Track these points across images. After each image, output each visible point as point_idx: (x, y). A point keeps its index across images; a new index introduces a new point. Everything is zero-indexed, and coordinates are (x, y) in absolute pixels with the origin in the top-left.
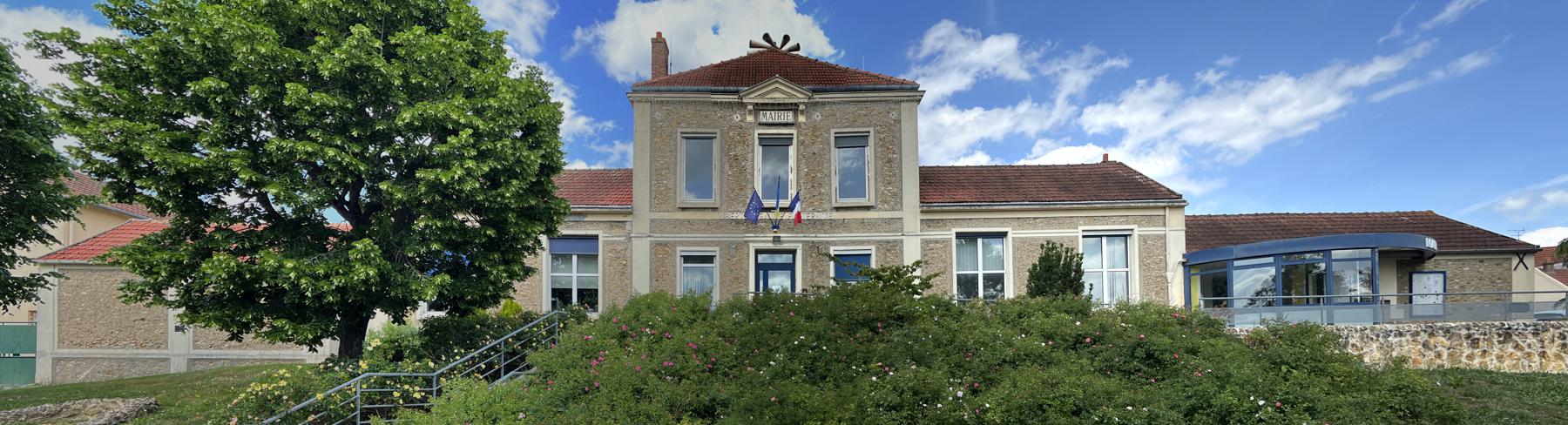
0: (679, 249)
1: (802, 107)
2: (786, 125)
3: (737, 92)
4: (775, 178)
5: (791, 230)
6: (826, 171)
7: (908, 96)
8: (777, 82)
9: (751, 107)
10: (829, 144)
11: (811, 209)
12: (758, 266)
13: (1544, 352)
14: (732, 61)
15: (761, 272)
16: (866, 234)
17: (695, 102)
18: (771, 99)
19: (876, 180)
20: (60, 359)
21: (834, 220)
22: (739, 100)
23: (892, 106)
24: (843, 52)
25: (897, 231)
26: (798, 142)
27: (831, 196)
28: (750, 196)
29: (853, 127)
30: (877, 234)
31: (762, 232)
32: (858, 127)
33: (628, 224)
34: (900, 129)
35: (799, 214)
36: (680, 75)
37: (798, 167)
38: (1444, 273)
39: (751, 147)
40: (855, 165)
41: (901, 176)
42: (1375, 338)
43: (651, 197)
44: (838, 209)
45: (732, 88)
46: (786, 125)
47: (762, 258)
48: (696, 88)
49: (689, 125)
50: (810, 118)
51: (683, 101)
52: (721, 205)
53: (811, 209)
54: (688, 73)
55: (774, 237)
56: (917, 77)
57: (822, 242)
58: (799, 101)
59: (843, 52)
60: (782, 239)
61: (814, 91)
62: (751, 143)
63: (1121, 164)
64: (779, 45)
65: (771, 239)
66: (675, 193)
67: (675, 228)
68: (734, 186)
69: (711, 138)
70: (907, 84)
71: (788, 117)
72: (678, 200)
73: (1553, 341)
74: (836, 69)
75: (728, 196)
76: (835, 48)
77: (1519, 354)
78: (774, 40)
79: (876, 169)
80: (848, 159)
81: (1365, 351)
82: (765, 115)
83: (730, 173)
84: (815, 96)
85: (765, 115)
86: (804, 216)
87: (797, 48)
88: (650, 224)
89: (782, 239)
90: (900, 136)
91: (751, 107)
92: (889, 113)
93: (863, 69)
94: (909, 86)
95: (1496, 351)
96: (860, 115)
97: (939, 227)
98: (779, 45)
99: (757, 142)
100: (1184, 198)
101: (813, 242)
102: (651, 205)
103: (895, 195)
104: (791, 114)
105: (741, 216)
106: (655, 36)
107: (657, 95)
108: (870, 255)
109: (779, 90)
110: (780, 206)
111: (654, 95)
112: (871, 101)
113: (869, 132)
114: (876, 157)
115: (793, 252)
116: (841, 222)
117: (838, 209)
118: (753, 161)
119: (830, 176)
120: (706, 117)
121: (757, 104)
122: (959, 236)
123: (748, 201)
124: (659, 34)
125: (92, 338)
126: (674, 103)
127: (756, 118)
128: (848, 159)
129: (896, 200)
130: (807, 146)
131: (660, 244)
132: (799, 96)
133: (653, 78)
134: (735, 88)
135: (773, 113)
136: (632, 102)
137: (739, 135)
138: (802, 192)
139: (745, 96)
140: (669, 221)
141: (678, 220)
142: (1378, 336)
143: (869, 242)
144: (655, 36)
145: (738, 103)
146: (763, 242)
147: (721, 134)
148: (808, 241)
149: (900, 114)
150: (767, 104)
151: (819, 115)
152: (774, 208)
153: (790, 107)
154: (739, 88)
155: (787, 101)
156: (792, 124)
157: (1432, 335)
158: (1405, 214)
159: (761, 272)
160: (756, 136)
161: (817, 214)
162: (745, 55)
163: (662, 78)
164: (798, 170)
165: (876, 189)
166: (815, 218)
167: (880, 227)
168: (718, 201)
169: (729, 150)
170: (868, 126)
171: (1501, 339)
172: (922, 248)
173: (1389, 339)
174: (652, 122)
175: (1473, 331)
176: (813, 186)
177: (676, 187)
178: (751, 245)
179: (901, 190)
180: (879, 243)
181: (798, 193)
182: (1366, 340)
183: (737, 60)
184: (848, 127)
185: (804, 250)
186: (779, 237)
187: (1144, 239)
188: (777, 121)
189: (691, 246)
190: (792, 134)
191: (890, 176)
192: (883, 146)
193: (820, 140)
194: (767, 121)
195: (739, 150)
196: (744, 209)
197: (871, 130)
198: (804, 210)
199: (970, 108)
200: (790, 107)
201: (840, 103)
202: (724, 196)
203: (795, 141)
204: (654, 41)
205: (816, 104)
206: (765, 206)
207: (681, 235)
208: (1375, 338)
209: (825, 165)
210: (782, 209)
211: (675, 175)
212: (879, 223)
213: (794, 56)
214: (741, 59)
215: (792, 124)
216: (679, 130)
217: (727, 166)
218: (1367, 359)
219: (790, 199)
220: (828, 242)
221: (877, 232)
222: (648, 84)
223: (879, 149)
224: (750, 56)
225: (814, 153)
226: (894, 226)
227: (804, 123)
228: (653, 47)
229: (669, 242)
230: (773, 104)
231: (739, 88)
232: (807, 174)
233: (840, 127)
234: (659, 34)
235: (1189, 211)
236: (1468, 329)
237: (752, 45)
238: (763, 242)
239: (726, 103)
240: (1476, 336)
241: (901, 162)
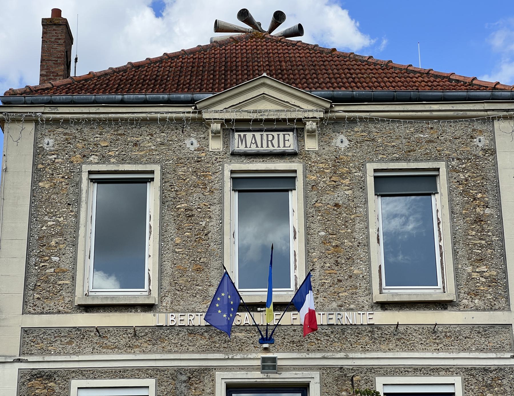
1: (310, 125)
2: (282, 155)
3: (192, 102)
4: (264, 248)
5: (297, 345)
6: (360, 237)
7: (507, 110)
8: (264, 85)
9: (216, 127)
10: (364, 189)
11: (334, 305)
14: (184, 53)
16: (441, 355)
17: (116, 120)
18: (255, 112)
19: (455, 253)
21: (379, 327)
22: (196, 115)
23: (478, 126)
24: (385, 42)
26: (306, 184)
27: (370, 282)
28: (216, 283)
30: (462, 355)
31: (241, 350)
32: (416, 160)
34: (495, 164)
35: (311, 315)
36: (91, 77)
37: (307, 228)
39: (217, 194)
40: (410, 227)
41: (503, 247)
43: (26, 286)
44: (384, 306)
45: (182, 96)
46: (282, 155)
48: (119, 97)
49: (104, 159)
50: (329, 144)
51: (94, 120)
52: (161, 299)
53: (334, 305)
54: (105, 74)
55: (264, 360)
57: (358, 369)
58: (306, 115)
59: (385, 42)
60: (279, 363)
61: (336, 100)
62: (217, 186)
64: (266, 27)
65: (259, 363)
66: (73, 278)
67: (70, 343)
68: (186, 264)
69: (145, 181)
70: (501, 90)
72: (79, 292)
74: (369, 64)
75: (174, 283)
76: (372, 38)
78: (256, 19)
79: (454, 234)
80: (395, 216)
82: (243, 140)
83: (178, 240)
84: (337, 108)
85: (243, 140)
86: (321, 319)
87: (299, 31)
88: (22, 337)
89: (279, 363)
90: (497, 177)
91: (216, 127)
92: (472, 137)
93: (420, 65)
96: (418, 141)
98: (266, 27)
99: (228, 184)
101: (341, 368)
102: (25, 303)
103: (492, 281)
104: (291, 137)
105: (199, 320)
106: (49, 16)
107: (47, 110)
110: (274, 300)
111: (42, 110)
112: (439, 118)
113: (438, 170)
114: (452, 212)
116: (392, 329)
117: (384, 306)
118: (222, 219)
119: (368, 245)
120: (136, 145)
121: (228, 121)
123: (212, 291)
124: (57, 12)
126: (78, 122)
127: (226, 144)
128: (395, 216)
130: (324, 191)
133: (42, 82)
134: (189, 96)
135: (258, 135)
138: (315, 275)
139: (207, 107)
140: (58, 331)
141: (78, 329)
143: (447, 370)
144: (49, 16)
145: (193, 119)
146: (242, 368)
147: (163, 174)
148: (330, 367)
149: (493, 140)
150: (247, 121)
151: (345, 139)
152: (262, 305)
153: (288, 125)
154: (197, 96)
155: (283, 116)
156: (293, 155)
160: (227, 174)
161: (346, 314)
162: (206, 42)
163: (58, 82)
164: (307, 234)
165: (456, 269)
166: (344, 322)
167: (470, 342)
168: (155, 294)
169: (177, 199)
170: (436, 159)
176: (337, 263)
177: (74, 269)
178: (219, 375)
179: (505, 272)
180: (320, 368)
181: (308, 276)
183: (192, 52)
184: (398, 160)
185: (323, 384)
186: (274, 359)
188: (264, 149)
189: (100, 377)
190: (295, 171)
191: (482, 247)
193: (347, 181)
194: (248, 150)
196: (205, 307)
197: (442, 166)
198: (322, 307)
200: (288, 125)
201: (382, 120)
202: (166, 283)
203: (299, 183)
204: (46, 23)
205: (338, 121)
206: (246, 300)
207: (81, 358)
209: (357, 226)
210: (280, 307)
211: (75, 245)
212: (467, 333)
213: (294, 44)
214: (200, 50)
215: (293, 155)
216: (86, 168)
217: (172, 228)
219: (293, 287)
220: (372, 369)
221: (464, 350)
222: (30, 91)
223: (458, 199)
224: (215, 45)
225: (337, 205)
226: (494, 340)
227: (316, 153)
228: (44, 33)
229: (56, 372)
230: (256, 121)
231: (197, 96)
232: (325, 241)
233: (382, 160)
234: (57, 12)
237: (218, 28)
238: (242, 368)
239: (171, 119)
241: (501, 222)
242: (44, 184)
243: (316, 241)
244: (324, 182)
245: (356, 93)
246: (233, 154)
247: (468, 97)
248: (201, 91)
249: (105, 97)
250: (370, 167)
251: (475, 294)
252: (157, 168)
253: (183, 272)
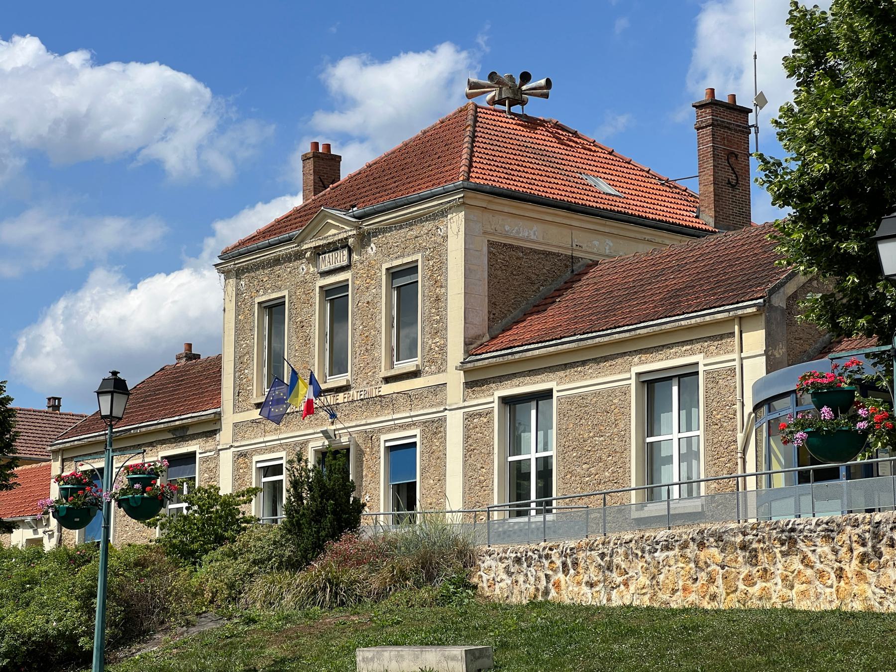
0: (383, 437)
13: (841, 569)
42: (640, 554)
56: (292, 204)
73: (851, 550)
77: (809, 572)
81: (630, 574)
88: (234, 430)
95: (779, 569)
97: (483, 391)
108: (415, 443)
117: (388, 380)
122: (506, 401)
142: (643, 551)
157: (702, 545)
171: (784, 548)
173: (656, 555)
174: (237, 295)
175: (750, 537)
182: (631, 557)
199: (58, 300)
208: (640, 554)
225: (368, 303)
235: (312, 397)
236: (745, 534)
240: (755, 545)
250: (418, 257)
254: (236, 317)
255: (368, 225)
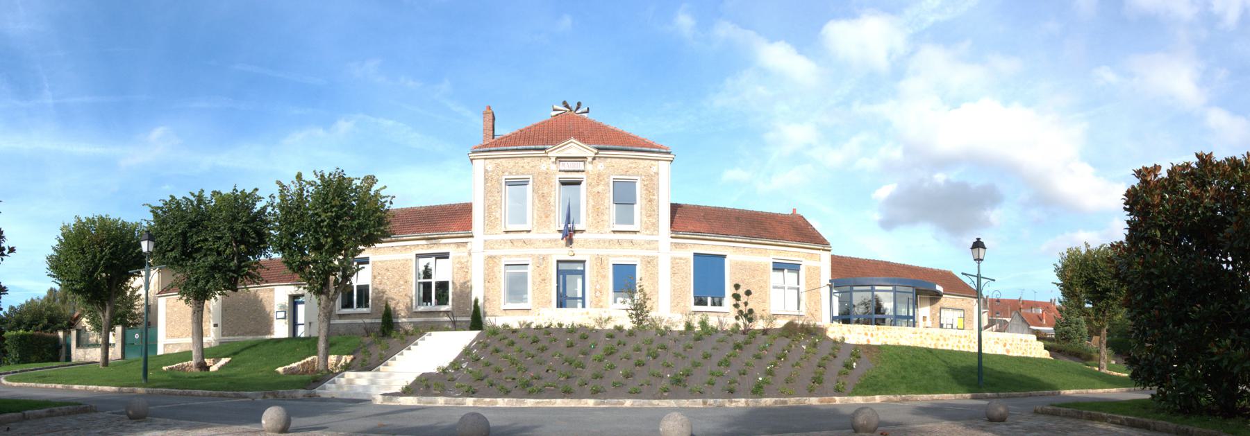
3: (544, 149)
12: (559, 272)
15: (561, 276)
20: (167, 344)
25: (654, 249)
29: (626, 175)
32: (629, 175)
33: (469, 244)
38: (940, 308)
39: (553, 187)
41: (658, 212)
43: (484, 224)
47: (563, 267)
48: (515, 147)
61: (599, 149)
63: (802, 217)
64: (574, 109)
69: (579, 183)
71: (580, 166)
94: (665, 151)
100: (831, 245)
102: (484, 231)
103: (653, 224)
109: (573, 148)
115: (583, 262)
125: (179, 334)
129: (655, 226)
130: (594, 187)
131: (490, 257)
132: (589, 152)
136: (472, 160)
137: (545, 178)
147: (533, 179)
154: (546, 146)
158: (940, 271)
159: (561, 276)
170: (528, 174)
172: (672, 262)
187: (808, 269)
192: (646, 190)
195: (545, 190)
197: (531, 177)
203: (531, 182)
217: (537, 201)
218: (458, 429)
225: (598, 192)
226: (652, 246)
231: (546, 146)
233: (616, 175)
235: (832, 253)
242: (489, 184)
243: (590, 206)
244: (594, 183)
245: (608, 146)
246: (560, 171)
247: (1125, 195)
248: (547, 145)
249: (510, 148)
250: (612, 177)
251: (647, 228)
252: (531, 177)
253: (541, 218)
254: (485, 184)
255: (602, 153)
